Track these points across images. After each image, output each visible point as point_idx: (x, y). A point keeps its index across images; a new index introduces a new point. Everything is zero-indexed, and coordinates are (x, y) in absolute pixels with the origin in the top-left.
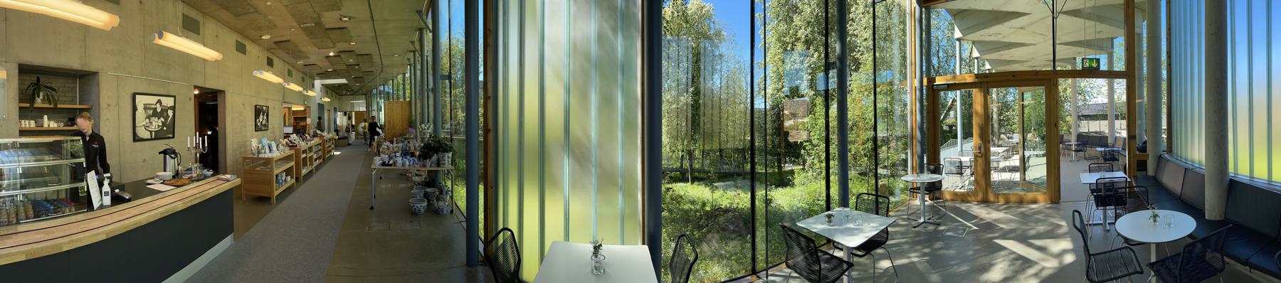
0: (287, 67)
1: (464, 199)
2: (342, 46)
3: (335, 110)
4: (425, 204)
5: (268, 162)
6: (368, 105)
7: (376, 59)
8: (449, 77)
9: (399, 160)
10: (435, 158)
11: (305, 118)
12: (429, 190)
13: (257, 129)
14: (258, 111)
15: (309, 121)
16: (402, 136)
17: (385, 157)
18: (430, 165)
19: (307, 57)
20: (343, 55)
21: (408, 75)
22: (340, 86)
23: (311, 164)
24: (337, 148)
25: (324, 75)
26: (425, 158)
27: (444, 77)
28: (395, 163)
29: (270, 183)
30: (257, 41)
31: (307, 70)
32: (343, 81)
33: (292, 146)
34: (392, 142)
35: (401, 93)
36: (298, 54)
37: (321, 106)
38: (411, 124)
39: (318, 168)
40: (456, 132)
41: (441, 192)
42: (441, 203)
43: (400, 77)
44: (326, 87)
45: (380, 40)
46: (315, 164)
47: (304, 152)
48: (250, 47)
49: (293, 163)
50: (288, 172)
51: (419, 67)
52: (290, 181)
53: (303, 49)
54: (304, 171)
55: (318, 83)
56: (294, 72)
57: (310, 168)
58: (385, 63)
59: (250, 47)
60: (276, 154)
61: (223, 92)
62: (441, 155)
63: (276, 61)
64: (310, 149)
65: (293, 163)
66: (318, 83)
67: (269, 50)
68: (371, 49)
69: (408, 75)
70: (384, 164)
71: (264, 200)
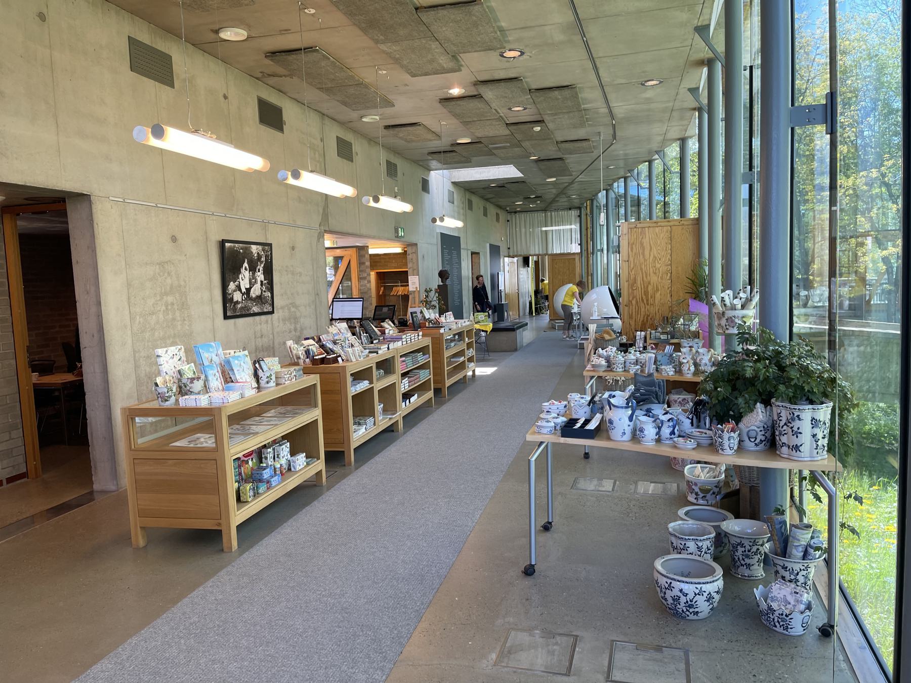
0: (333, 133)
1: (891, 640)
2: (480, 63)
3: (495, 251)
4: (715, 584)
5: (207, 420)
6: (587, 237)
7: (591, 97)
8: (829, 113)
9: (621, 420)
10: (757, 418)
11: (403, 277)
12: (733, 526)
13: (230, 310)
14: (231, 261)
15: (414, 283)
16: (666, 330)
17: (579, 404)
18: (737, 449)
19: (389, 104)
20: (488, 93)
21: (693, 146)
22: (503, 185)
23: (390, 408)
24: (482, 360)
25: (453, 155)
26: (721, 419)
27: (807, 115)
28: (601, 431)
29: (216, 486)
30: (208, 46)
31: (398, 139)
32: (509, 172)
33: (324, 362)
34: (624, 348)
35: (674, 198)
36: (359, 95)
37: (450, 243)
38: (699, 289)
39: (412, 419)
40: (860, 309)
41: (783, 546)
42: (780, 591)
43: (673, 151)
44: (468, 189)
45: (593, 31)
46: (404, 408)
47: (358, 376)
48: (183, 61)
49: (315, 414)
50: (299, 440)
51: (720, 112)
52: (304, 468)
53: (368, 76)
54: (360, 434)
55: (441, 179)
56: (358, 147)
57: (382, 421)
58: (621, 108)
59: (183, 61)
60: (244, 392)
61: (83, 198)
62: (781, 409)
63: (290, 112)
64: (386, 366)
65: (315, 414)
66: (441, 179)
67: (262, 77)
68: (566, 66)
69: (693, 146)
70: (569, 429)
71: (206, 539)
